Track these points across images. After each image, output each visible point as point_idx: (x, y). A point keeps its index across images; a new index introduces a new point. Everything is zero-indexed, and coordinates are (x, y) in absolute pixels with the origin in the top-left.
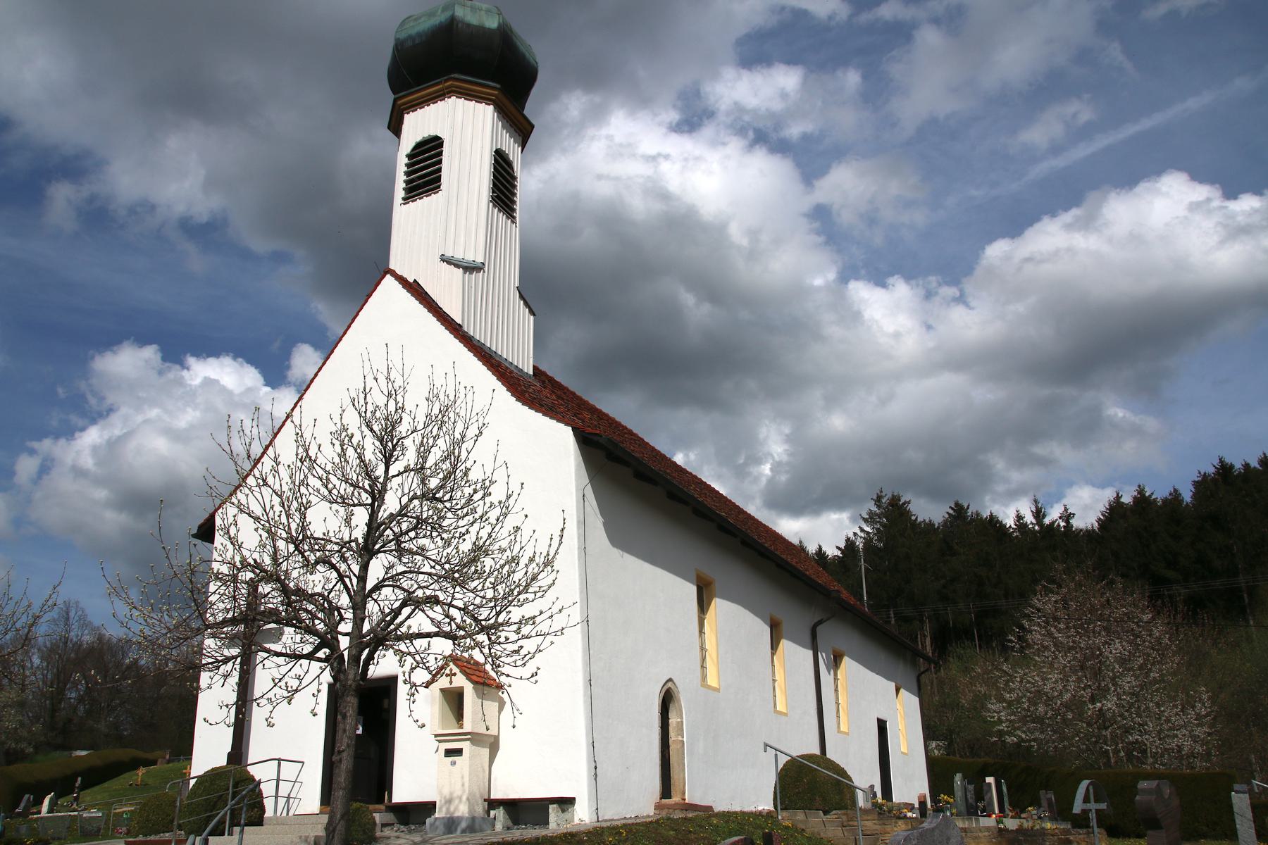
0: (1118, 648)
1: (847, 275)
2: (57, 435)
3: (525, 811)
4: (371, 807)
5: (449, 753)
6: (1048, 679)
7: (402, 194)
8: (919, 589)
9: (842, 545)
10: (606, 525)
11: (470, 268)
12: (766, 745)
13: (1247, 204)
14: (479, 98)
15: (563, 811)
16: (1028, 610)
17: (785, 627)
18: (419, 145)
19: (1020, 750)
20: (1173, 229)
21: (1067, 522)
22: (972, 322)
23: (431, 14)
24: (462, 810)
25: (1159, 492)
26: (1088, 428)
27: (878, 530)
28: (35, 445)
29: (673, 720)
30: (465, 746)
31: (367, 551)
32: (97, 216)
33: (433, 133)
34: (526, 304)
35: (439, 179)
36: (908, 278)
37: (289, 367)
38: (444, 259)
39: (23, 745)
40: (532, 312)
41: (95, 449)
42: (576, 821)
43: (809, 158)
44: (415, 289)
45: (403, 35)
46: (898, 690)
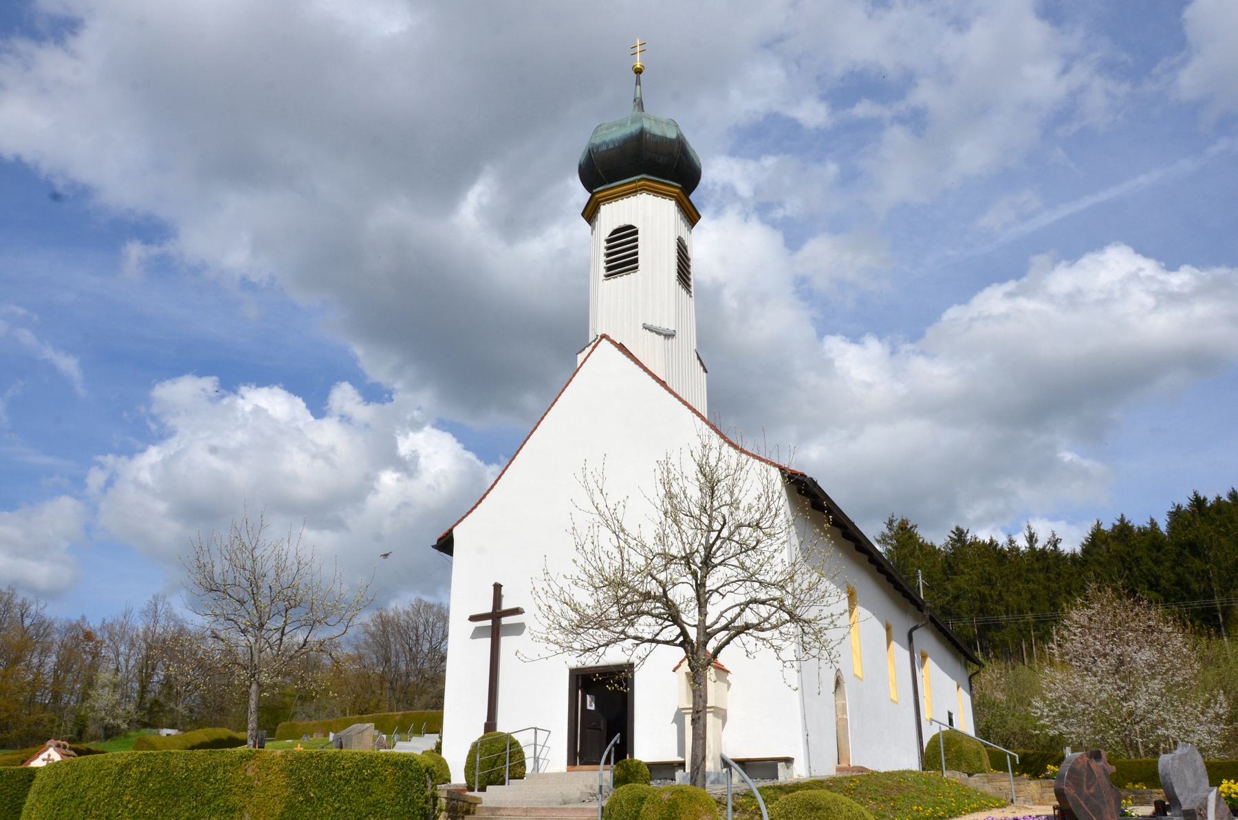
1: (825, 328)
2: (119, 453)
7: (603, 272)
11: (669, 335)
13: (1182, 279)
16: (1067, 622)
17: (893, 630)
20: (1123, 298)
21: (1055, 546)
22: (936, 374)
23: (621, 125)
25: (1139, 521)
26: (1043, 470)
27: (889, 551)
28: (100, 458)
32: (163, 268)
34: (702, 364)
35: (636, 261)
36: (880, 337)
38: (645, 327)
39: (119, 722)
40: (705, 371)
41: (152, 467)
43: (794, 235)
45: (597, 141)
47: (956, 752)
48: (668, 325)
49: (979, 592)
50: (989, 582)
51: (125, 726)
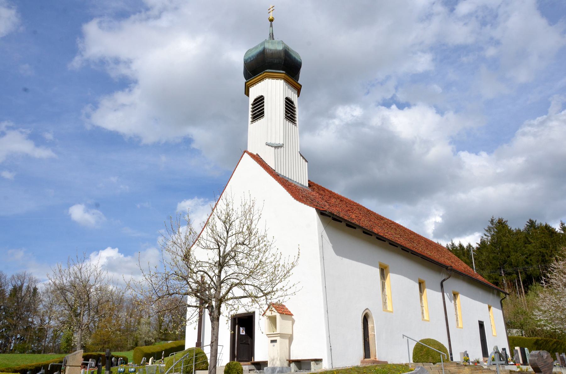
0: (177, 333)
3: (301, 364)
4: (241, 363)
5: (273, 341)
6: (561, 300)
8: (508, 261)
9: (479, 242)
10: (333, 247)
11: (277, 147)
12: (404, 335)
14: (277, 78)
15: (317, 364)
17: (426, 284)
18: (255, 100)
19: (552, 335)
23: (256, 48)
24: (278, 364)
29: (370, 325)
30: (278, 339)
31: (221, 265)
33: (260, 95)
34: (303, 158)
35: (263, 113)
37: (181, 202)
38: (267, 144)
39: (151, 339)
42: (323, 368)
44: (257, 158)
45: (247, 58)
46: (489, 308)
47: (426, 351)
48: (279, 141)
49: (540, 252)
50: (545, 246)
51: (153, 341)
